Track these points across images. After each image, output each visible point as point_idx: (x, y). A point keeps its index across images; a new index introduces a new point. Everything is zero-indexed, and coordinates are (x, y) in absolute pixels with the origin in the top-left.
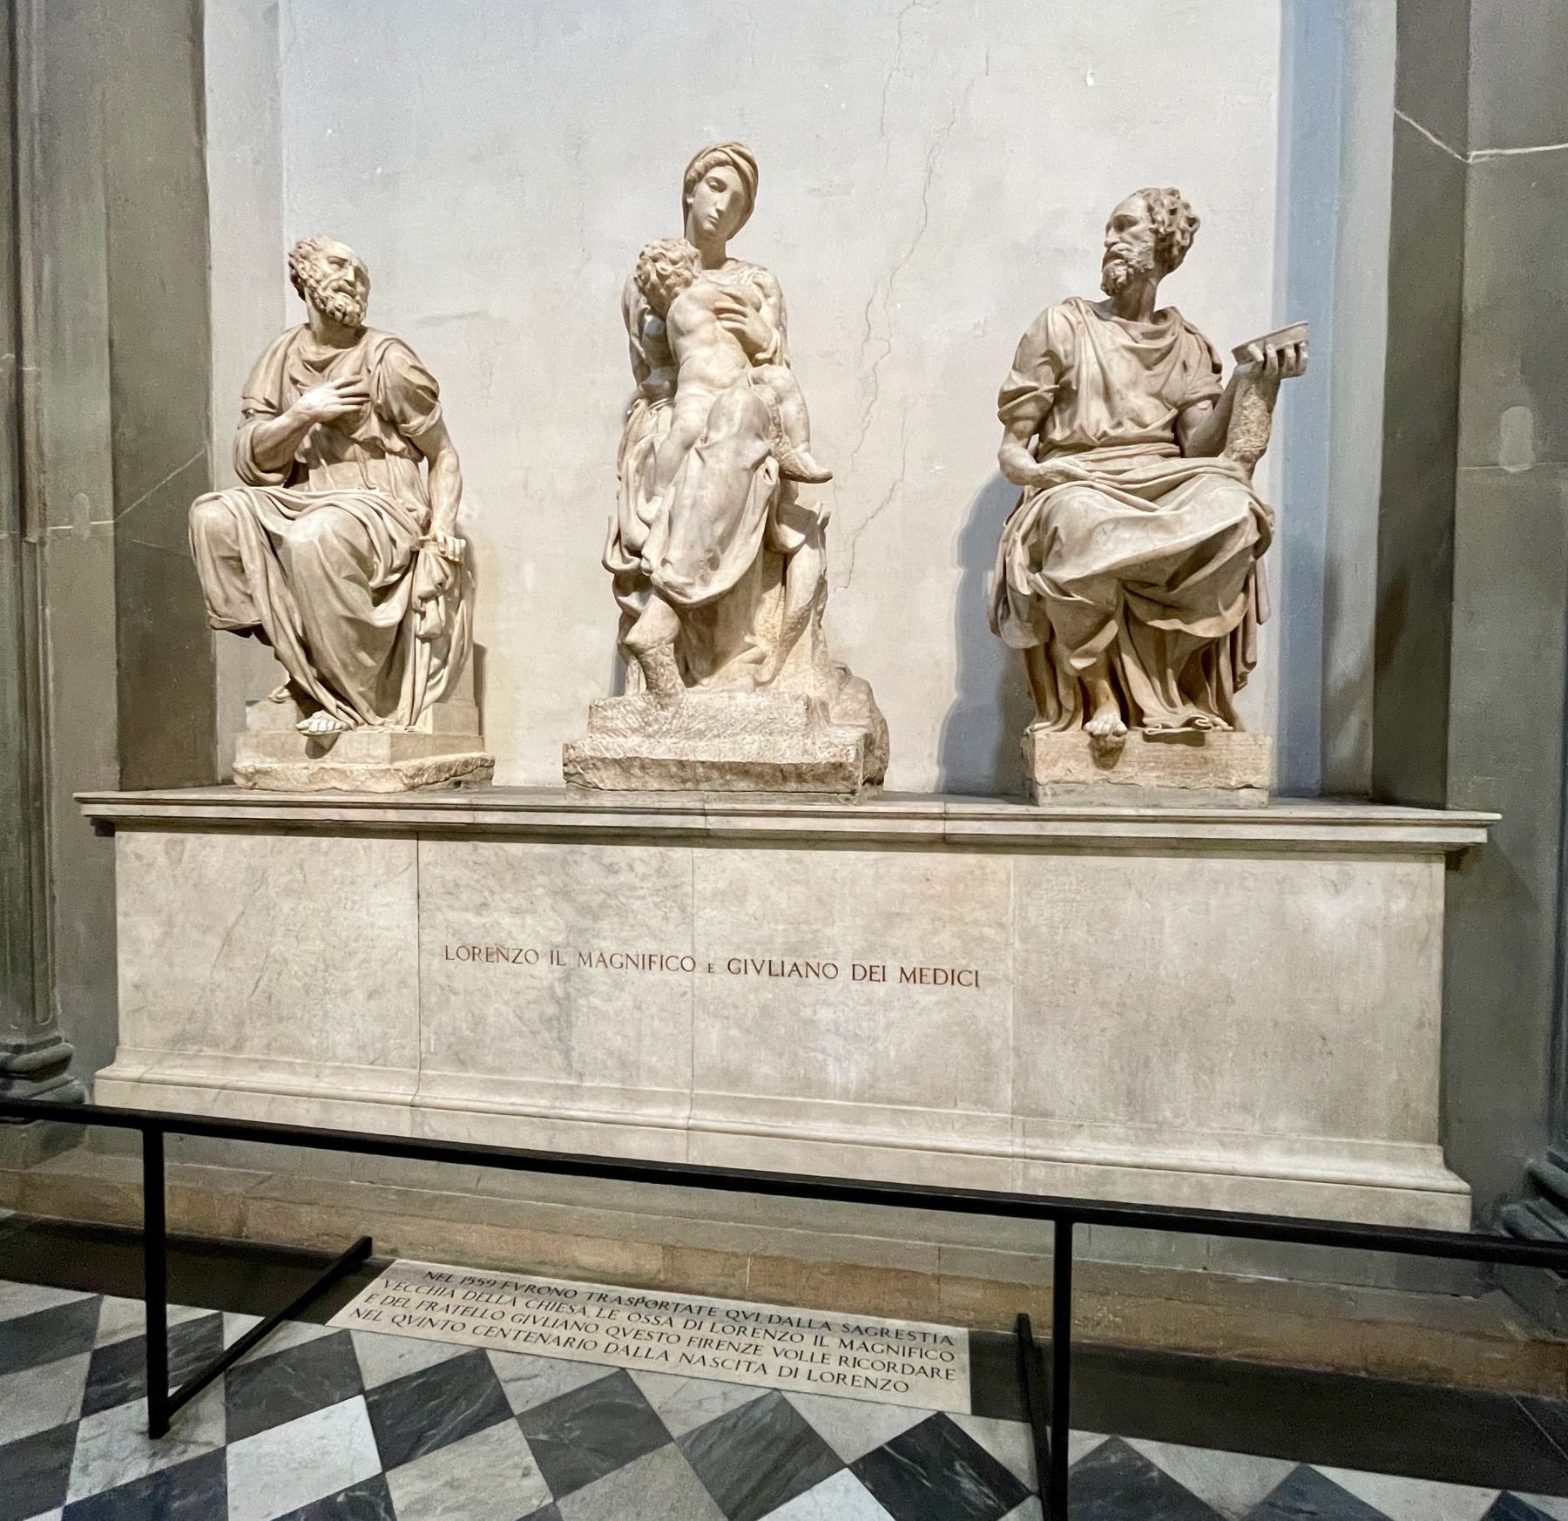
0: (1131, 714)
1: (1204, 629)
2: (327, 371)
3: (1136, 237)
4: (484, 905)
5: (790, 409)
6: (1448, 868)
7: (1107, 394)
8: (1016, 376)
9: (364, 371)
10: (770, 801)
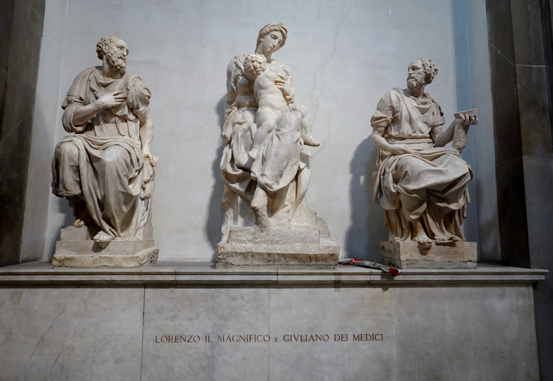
0: (431, 235)
1: (453, 206)
2: (108, 87)
3: (419, 73)
4: (175, 317)
5: (306, 120)
6: (534, 289)
7: (411, 121)
8: (378, 112)
9: (125, 89)
10: (304, 269)
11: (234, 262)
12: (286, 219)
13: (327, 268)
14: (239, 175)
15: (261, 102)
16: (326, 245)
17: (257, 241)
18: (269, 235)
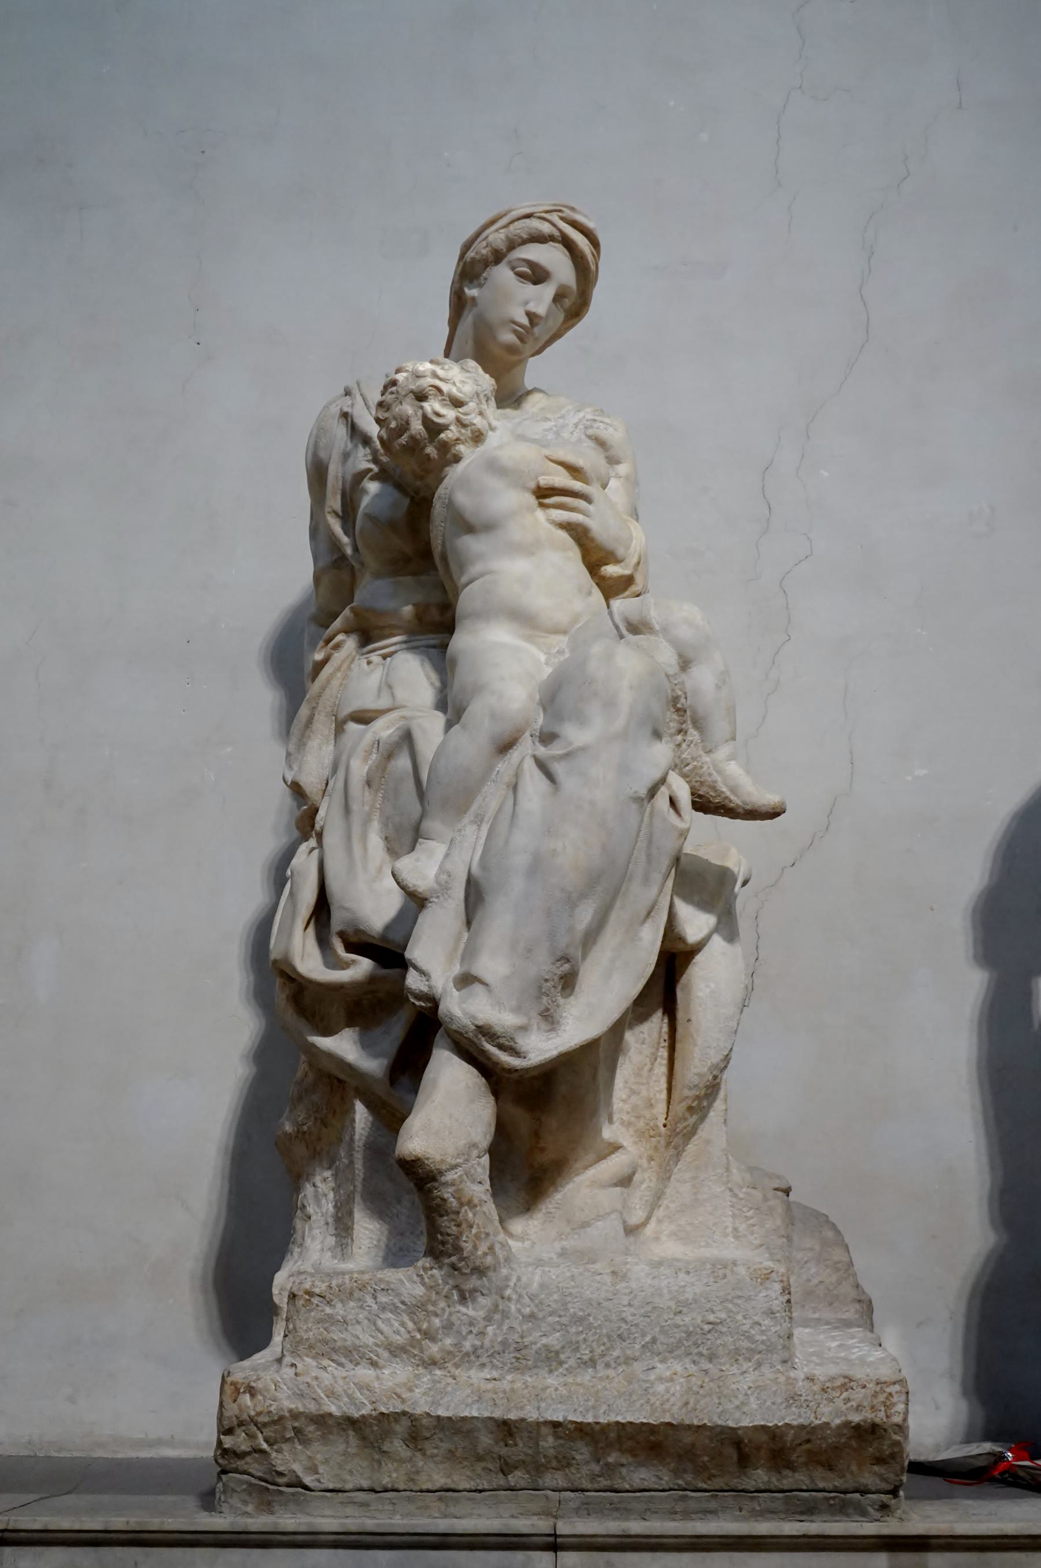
5: (703, 679)
11: (313, 1470)
12: (612, 1226)
13: (842, 1509)
14: (355, 985)
15: (468, 600)
16: (833, 1370)
17: (434, 1349)
18: (506, 1315)
